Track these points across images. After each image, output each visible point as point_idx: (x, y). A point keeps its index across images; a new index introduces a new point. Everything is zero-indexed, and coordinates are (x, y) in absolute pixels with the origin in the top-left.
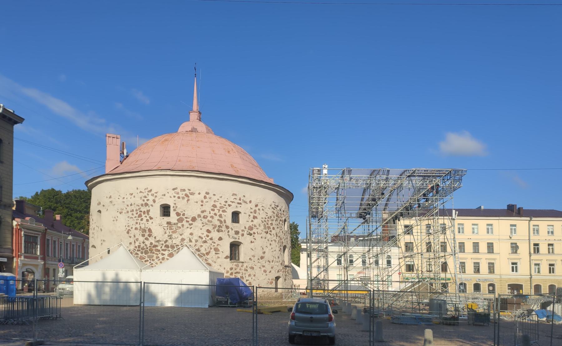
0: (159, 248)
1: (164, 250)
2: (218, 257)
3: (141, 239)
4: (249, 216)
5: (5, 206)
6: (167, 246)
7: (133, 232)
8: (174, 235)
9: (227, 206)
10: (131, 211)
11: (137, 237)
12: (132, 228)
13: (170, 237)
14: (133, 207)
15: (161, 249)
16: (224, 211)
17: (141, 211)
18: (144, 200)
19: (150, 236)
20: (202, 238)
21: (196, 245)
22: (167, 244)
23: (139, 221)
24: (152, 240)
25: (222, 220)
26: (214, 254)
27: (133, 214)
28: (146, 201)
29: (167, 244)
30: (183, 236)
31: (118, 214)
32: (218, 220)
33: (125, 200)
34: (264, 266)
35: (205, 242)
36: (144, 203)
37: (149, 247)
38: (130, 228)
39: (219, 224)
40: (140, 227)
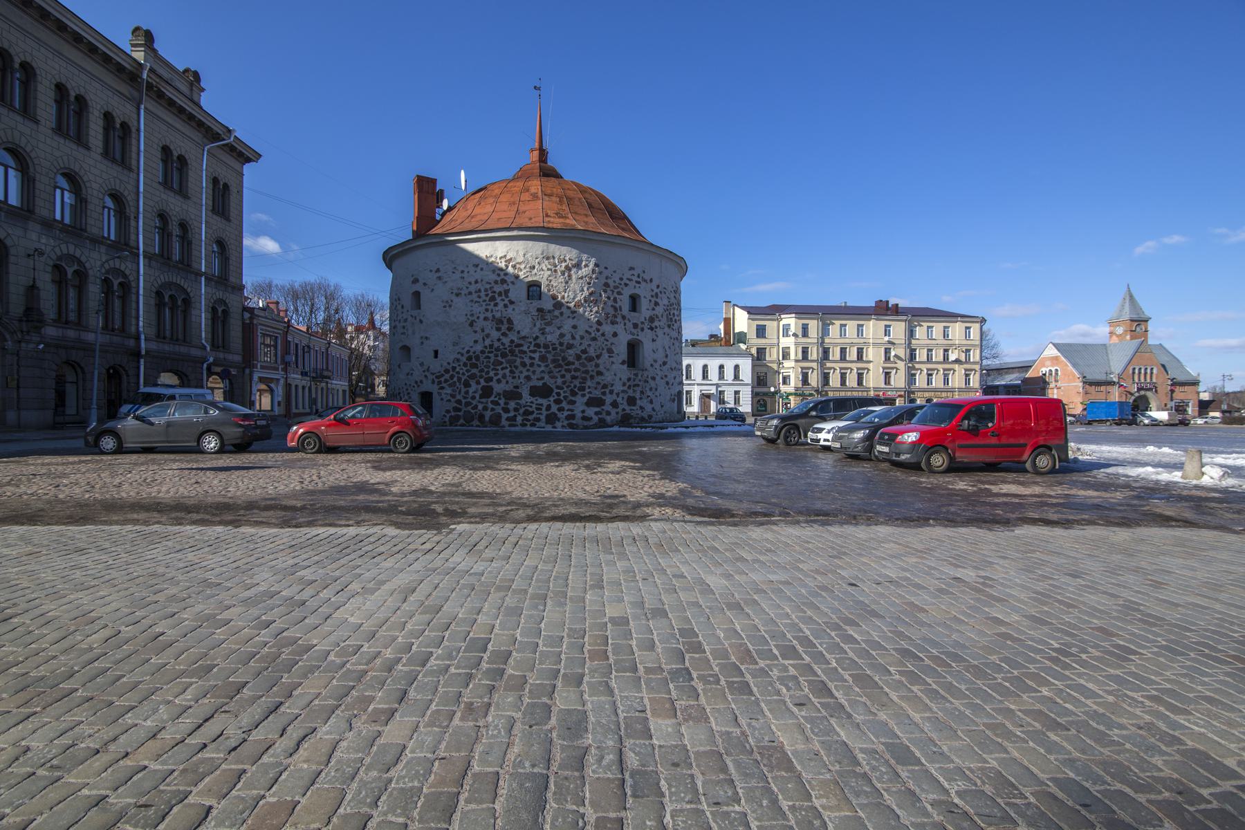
0: (525, 348)
1: (534, 352)
2: (613, 363)
3: (495, 334)
4: (650, 301)
5: (233, 288)
6: (538, 346)
7: (480, 324)
8: (548, 329)
9: (623, 286)
10: (476, 292)
11: (487, 331)
12: (478, 318)
13: (543, 332)
14: (479, 286)
16: (619, 293)
17: (495, 292)
18: (499, 275)
19: (510, 329)
20: (590, 334)
21: (581, 344)
22: (538, 341)
23: (489, 307)
24: (513, 336)
25: (617, 306)
26: (607, 357)
27: (479, 297)
28: (502, 277)
29: (538, 341)
30: (562, 330)
31: (453, 297)
32: (612, 306)
33: (465, 275)
34: (666, 376)
35: (594, 339)
36: (499, 279)
37: (509, 346)
38: (475, 318)
39: (613, 313)
40: (493, 316)
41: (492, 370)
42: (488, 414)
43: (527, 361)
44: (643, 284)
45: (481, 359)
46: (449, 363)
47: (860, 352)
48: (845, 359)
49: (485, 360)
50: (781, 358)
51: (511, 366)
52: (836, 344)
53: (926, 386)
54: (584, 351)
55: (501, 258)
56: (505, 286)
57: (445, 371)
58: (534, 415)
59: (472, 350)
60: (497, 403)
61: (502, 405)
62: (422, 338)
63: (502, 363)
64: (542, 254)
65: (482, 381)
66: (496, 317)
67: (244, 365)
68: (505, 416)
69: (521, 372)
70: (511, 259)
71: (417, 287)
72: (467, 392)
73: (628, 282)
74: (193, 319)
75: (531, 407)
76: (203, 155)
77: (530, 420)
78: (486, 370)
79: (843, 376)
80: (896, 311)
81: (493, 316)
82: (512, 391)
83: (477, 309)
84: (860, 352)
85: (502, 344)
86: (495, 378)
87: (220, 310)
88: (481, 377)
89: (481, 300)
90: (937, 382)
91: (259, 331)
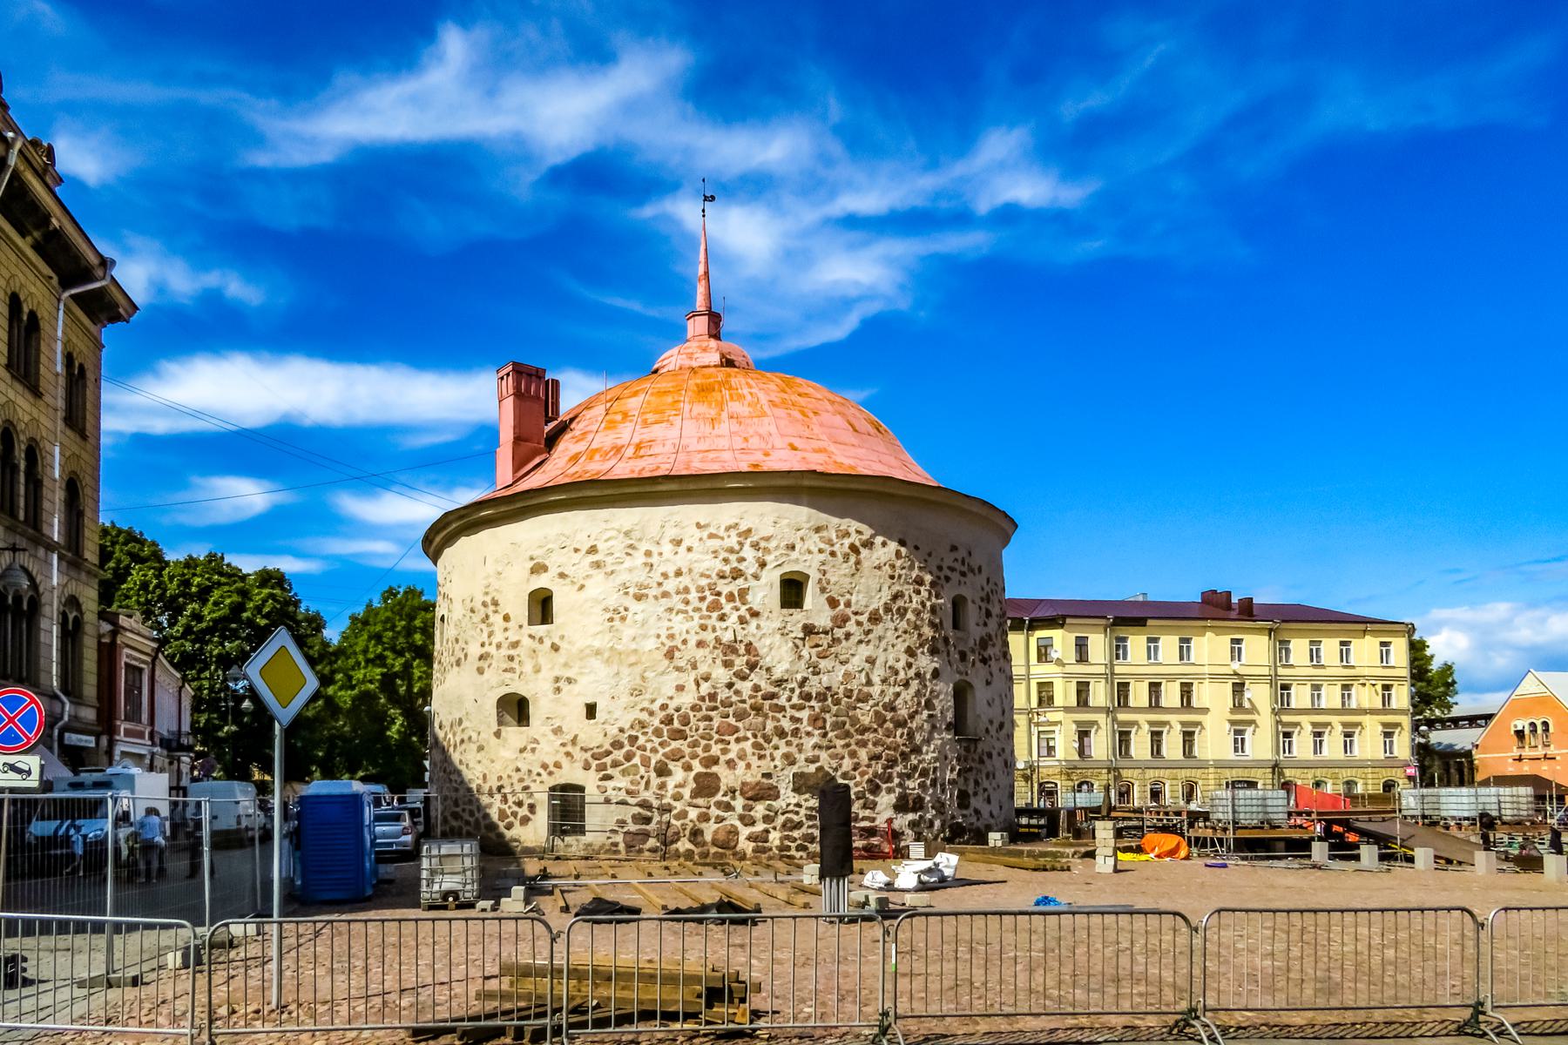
0: (782, 701)
1: (800, 708)
3: (721, 675)
4: (980, 608)
7: (690, 652)
8: (823, 664)
11: (703, 669)
12: (685, 642)
14: (685, 581)
15: (787, 705)
17: (719, 594)
27: (687, 603)
33: (655, 559)
37: (751, 697)
40: (717, 640)
41: (716, 743)
42: (709, 830)
43: (787, 725)
44: (970, 575)
45: (693, 721)
46: (622, 730)
47: (1186, 690)
48: (1086, 704)
49: (702, 725)
50: (1034, 703)
51: (755, 736)
52: (1139, 677)
53: (1311, 756)
54: (891, 707)
55: (728, 529)
56: (740, 581)
57: (612, 745)
58: (804, 830)
59: (672, 705)
60: (728, 807)
61: (739, 810)
62: (557, 680)
63: (737, 730)
64: (808, 522)
65: (696, 764)
66: (724, 640)
67: (100, 729)
68: (745, 832)
69: (776, 748)
70: (749, 531)
71: (542, 581)
72: (662, 786)
73: (949, 573)
74: (42, 639)
75: (797, 813)
76: (58, 309)
77: (795, 840)
78: (703, 742)
79: (1156, 737)
80: (1248, 611)
81: (717, 640)
82: (758, 783)
83: (679, 625)
84: (1186, 690)
85: (737, 693)
86: (723, 758)
87: (71, 617)
88: (694, 756)
89: (689, 608)
90: (1333, 748)
91: (125, 659)
